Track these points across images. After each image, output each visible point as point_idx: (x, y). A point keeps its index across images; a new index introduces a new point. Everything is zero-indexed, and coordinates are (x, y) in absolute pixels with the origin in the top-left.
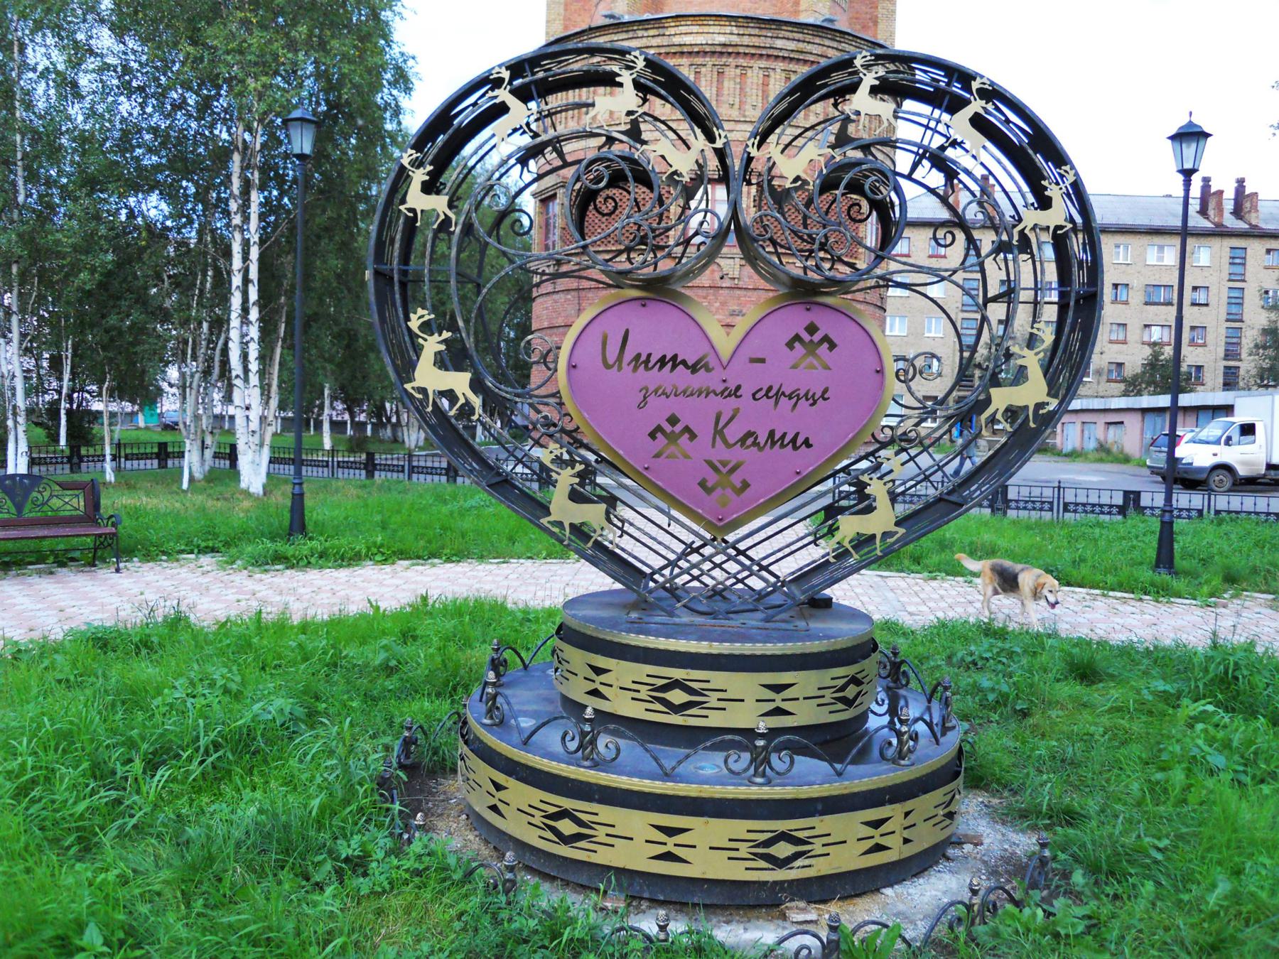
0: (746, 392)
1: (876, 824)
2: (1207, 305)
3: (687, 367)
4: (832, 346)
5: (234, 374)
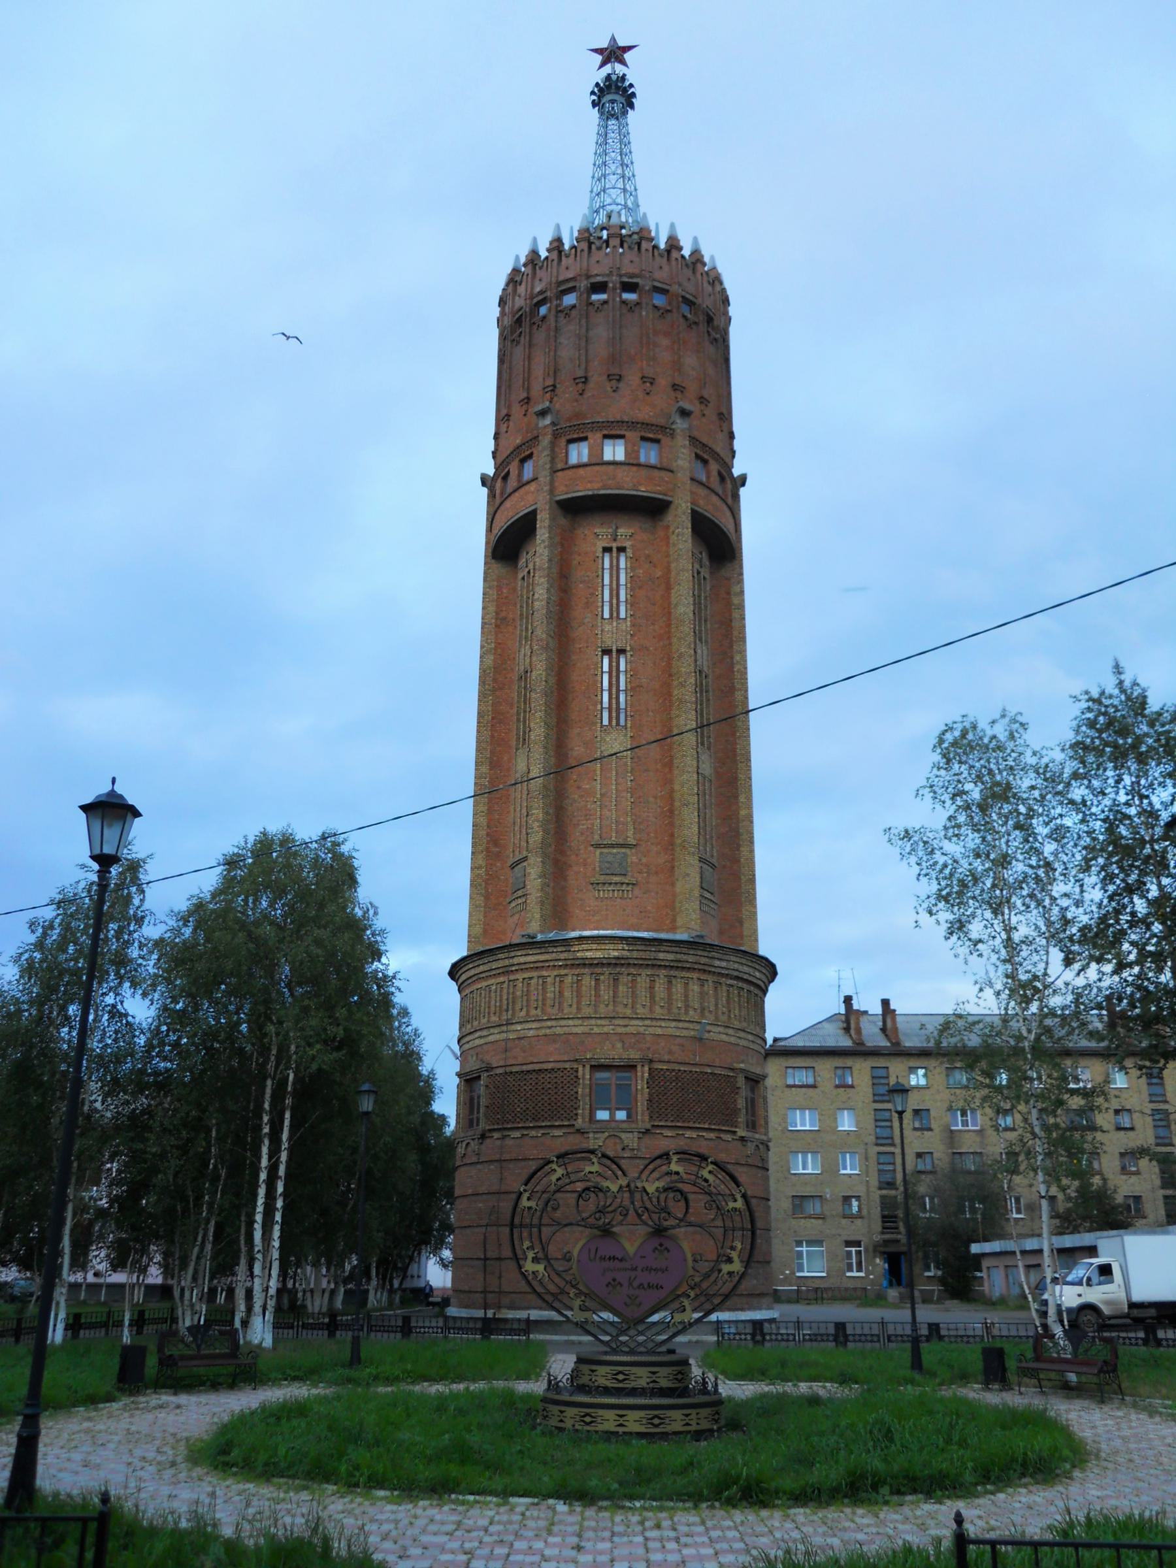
0: (639, 1269)
1: (687, 1415)
2: (1132, 1129)
5: (256, 1249)
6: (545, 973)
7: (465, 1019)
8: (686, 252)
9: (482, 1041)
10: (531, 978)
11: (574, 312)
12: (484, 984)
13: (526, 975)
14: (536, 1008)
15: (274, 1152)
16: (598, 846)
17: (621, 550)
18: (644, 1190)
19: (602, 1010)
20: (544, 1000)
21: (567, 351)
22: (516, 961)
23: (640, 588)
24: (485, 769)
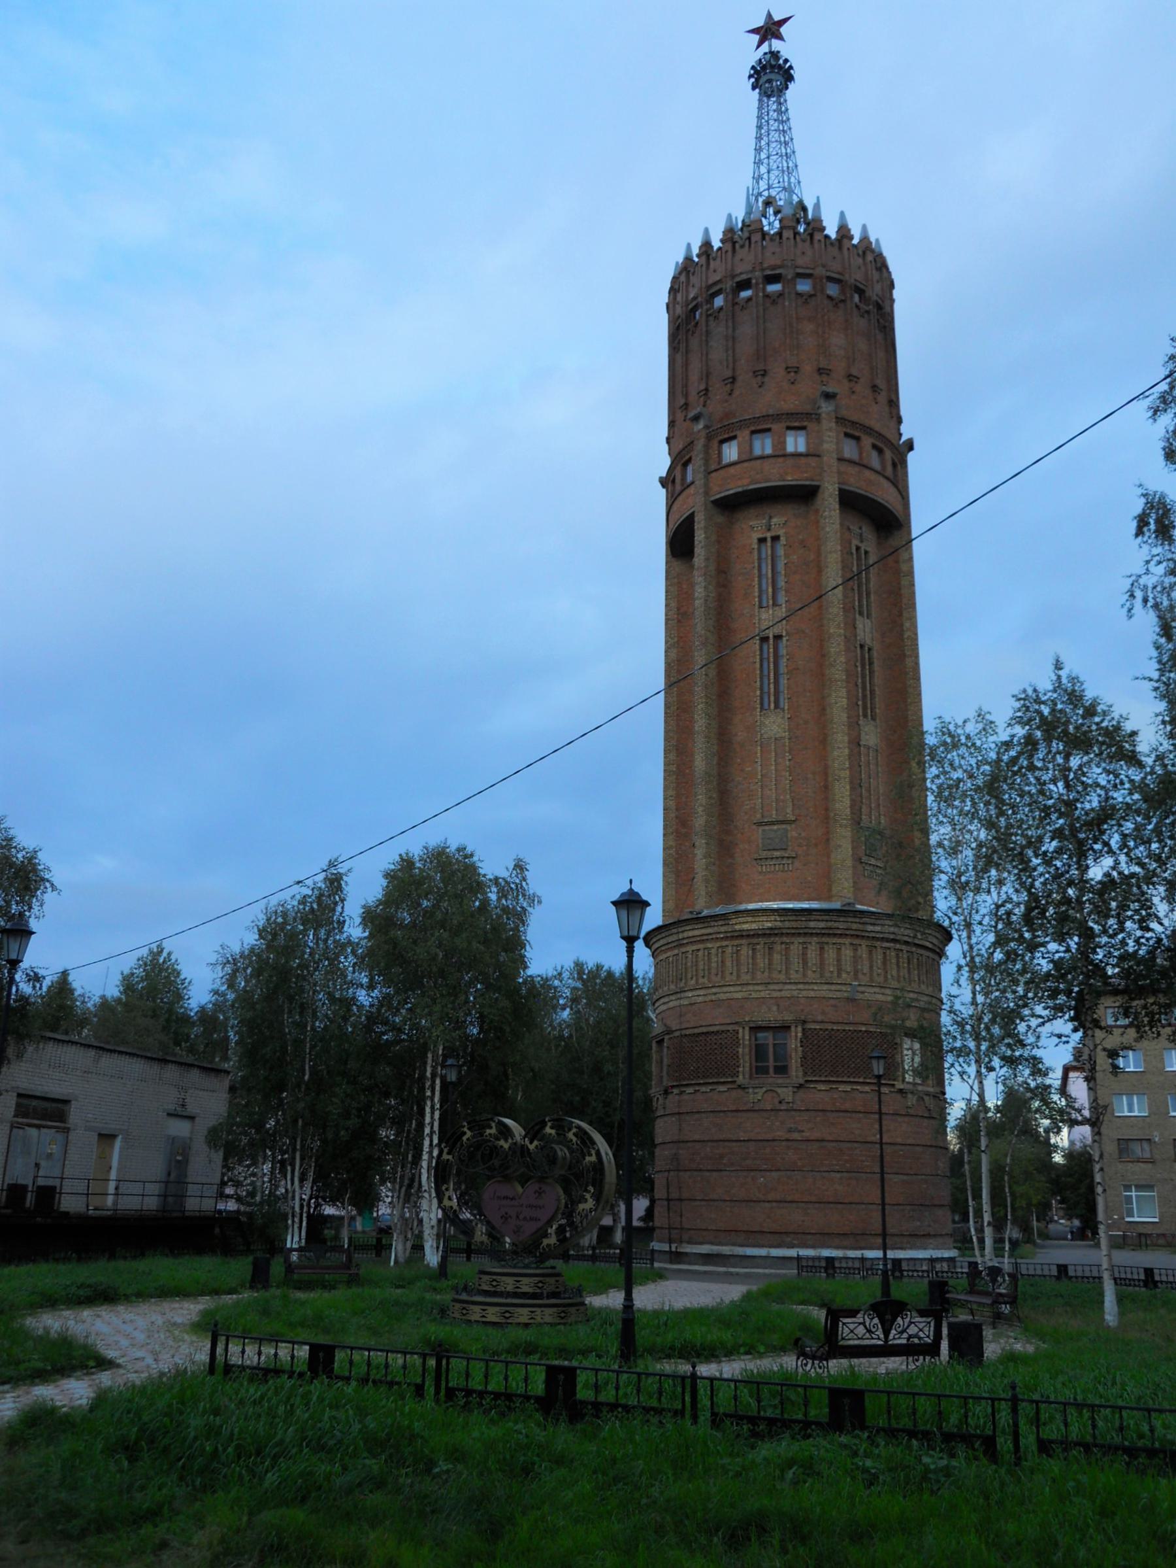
6: (709, 945)
8: (831, 231)
10: (698, 950)
11: (722, 314)
12: (665, 956)
14: (703, 977)
15: (432, 1113)
16: (760, 824)
19: (759, 977)
20: (709, 969)
21: (717, 353)
22: (686, 935)
24: (672, 756)
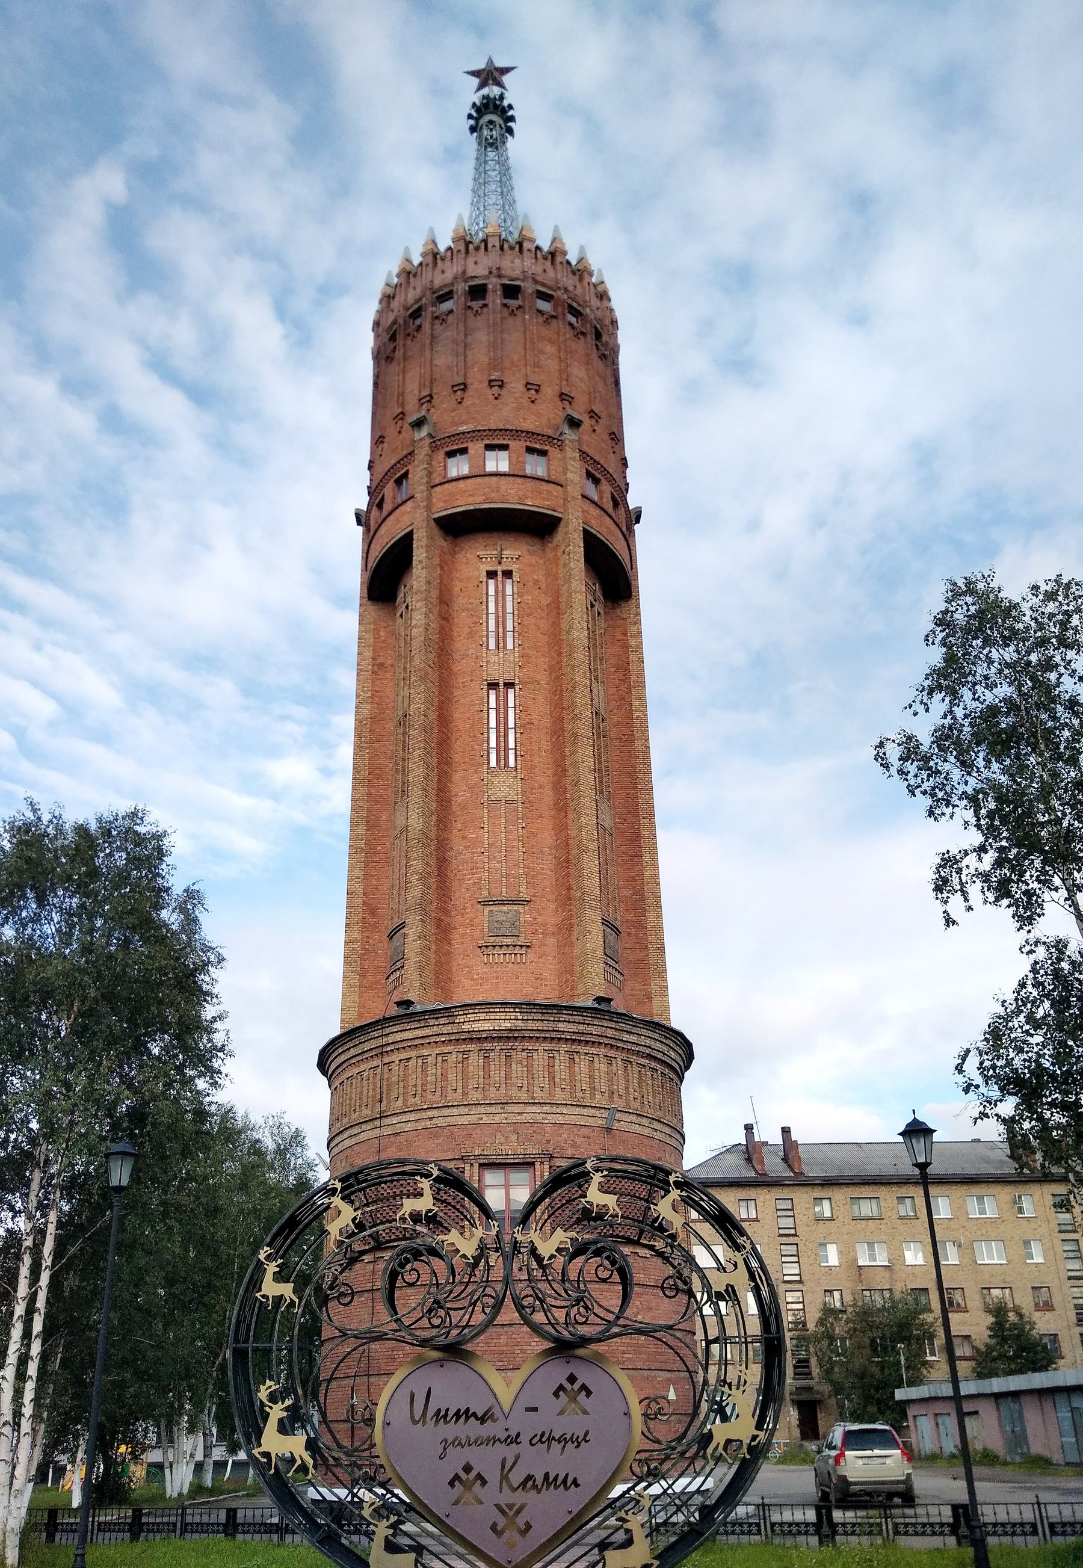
0: (524, 1439)
3: (477, 1418)
4: (589, 1393)
6: (425, 1052)
7: (335, 1118)
9: (353, 1141)
13: (404, 1055)
16: (485, 903)
17: (508, 574)
18: (533, 1251)
19: (493, 1095)
22: (391, 1039)
23: (529, 615)
24: (361, 830)
